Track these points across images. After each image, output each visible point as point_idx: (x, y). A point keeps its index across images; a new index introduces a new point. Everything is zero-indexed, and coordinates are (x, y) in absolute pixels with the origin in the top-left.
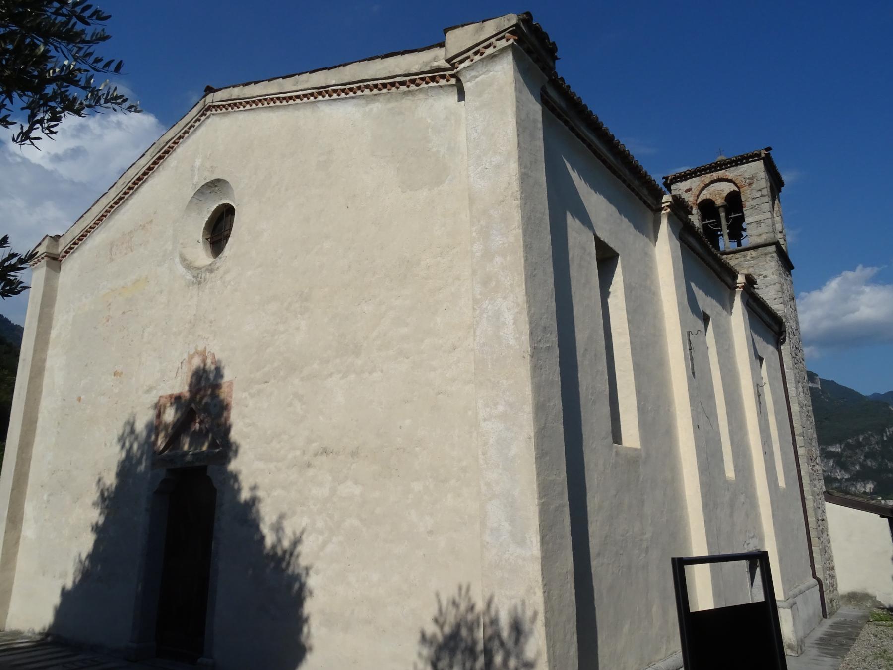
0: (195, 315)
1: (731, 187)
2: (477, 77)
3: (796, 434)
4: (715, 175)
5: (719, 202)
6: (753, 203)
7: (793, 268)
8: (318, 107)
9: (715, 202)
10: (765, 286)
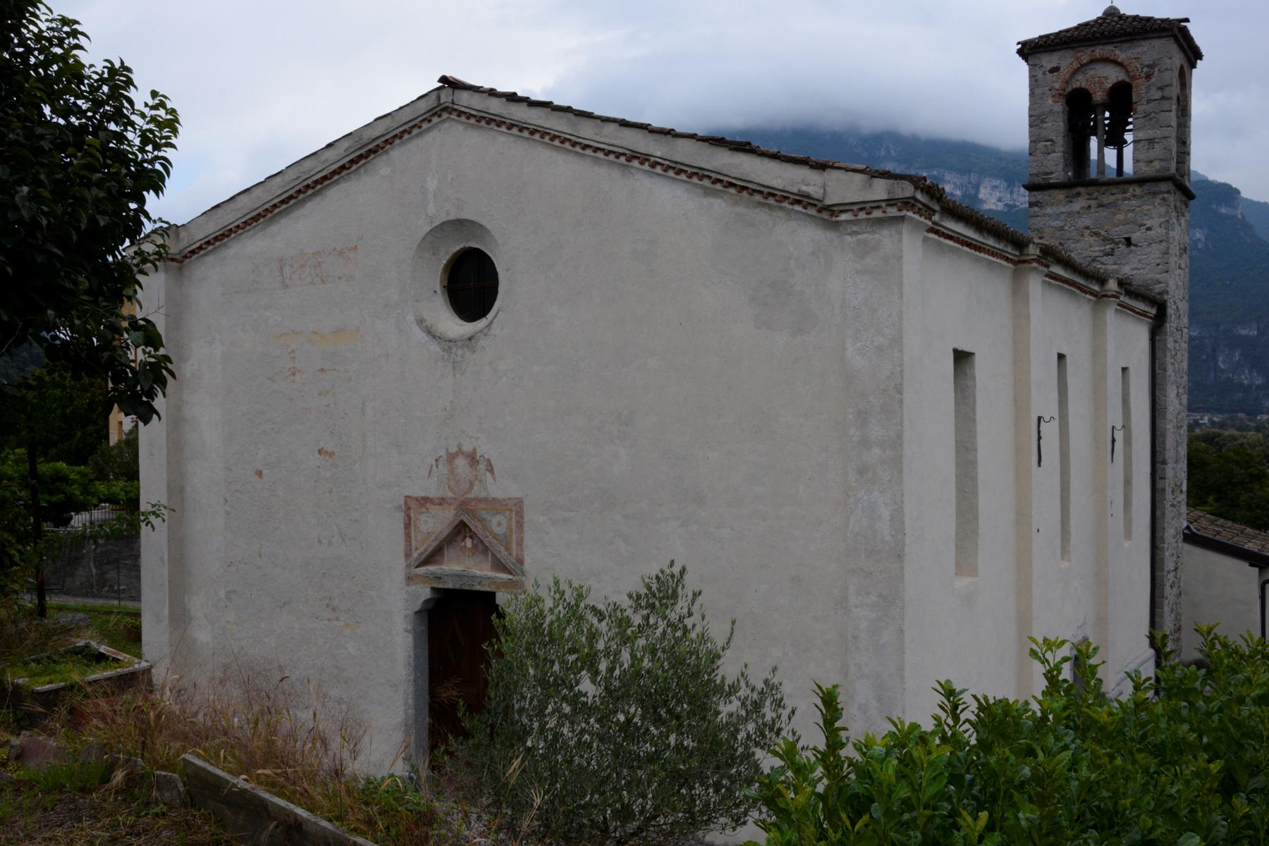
0: (451, 402)
2: (860, 234)
4: (1099, 51)
5: (1099, 96)
6: (1148, 108)
8: (631, 173)
9: (1093, 96)
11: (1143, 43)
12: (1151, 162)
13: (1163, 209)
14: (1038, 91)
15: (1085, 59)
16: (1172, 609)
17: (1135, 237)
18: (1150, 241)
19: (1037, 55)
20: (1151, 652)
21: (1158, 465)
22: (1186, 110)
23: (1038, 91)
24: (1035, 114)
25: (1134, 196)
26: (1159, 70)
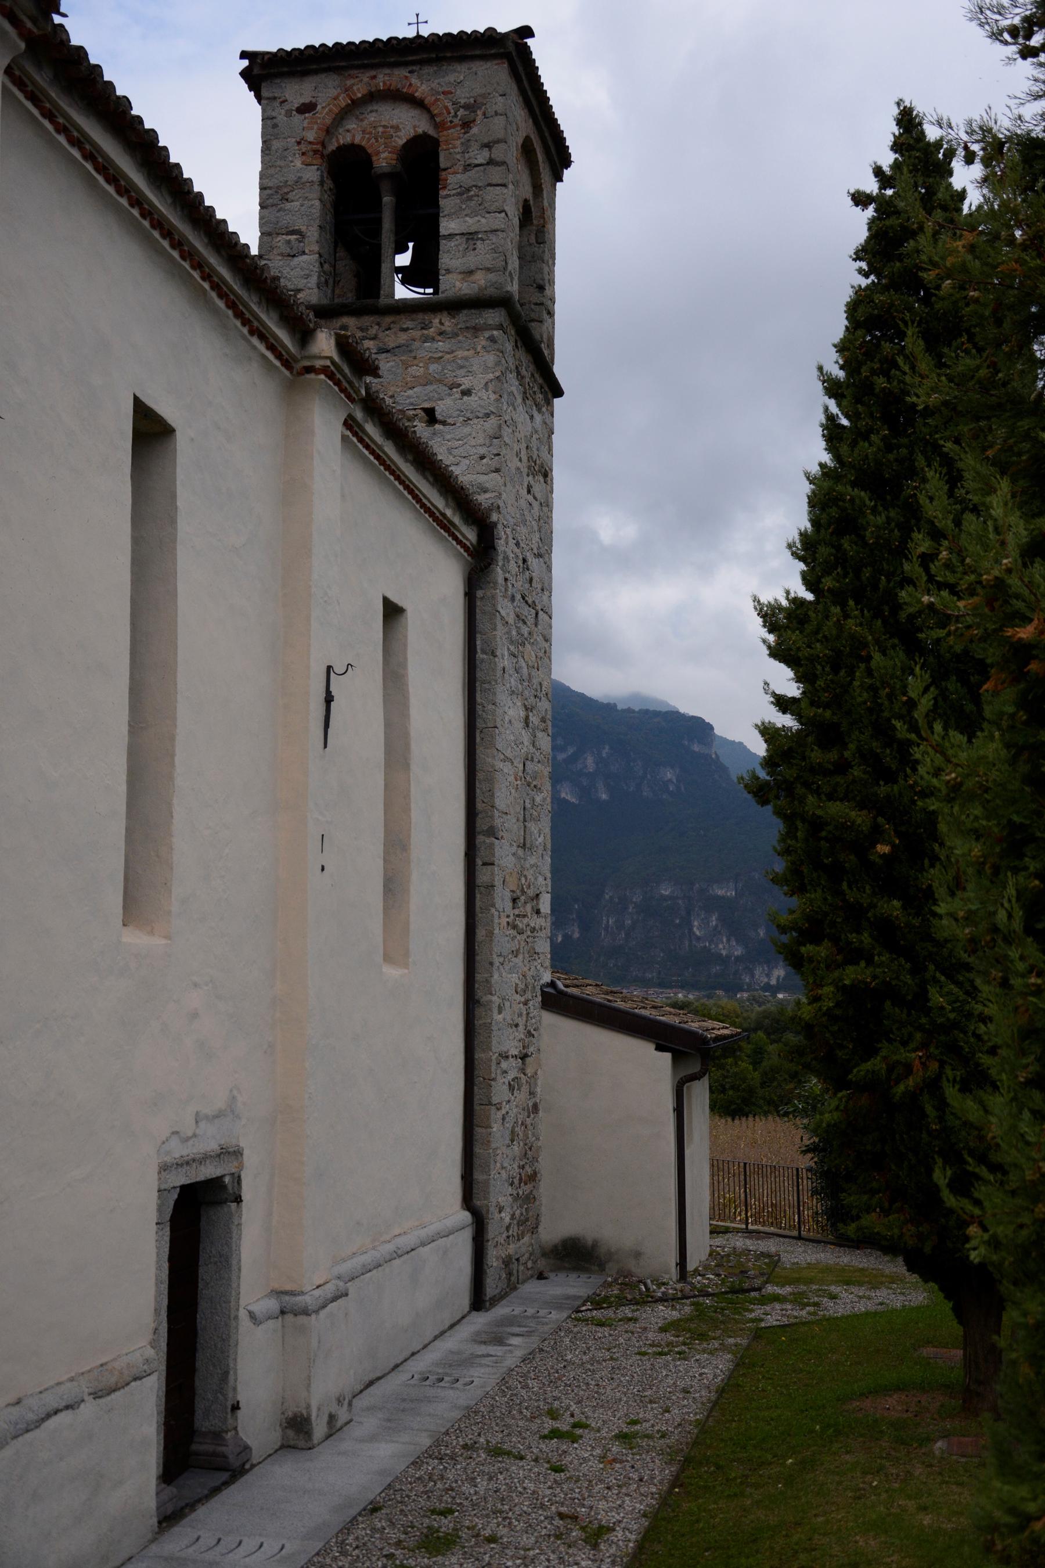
1: (423, 126)
3: (478, 829)
4: (384, 78)
5: (384, 160)
7: (558, 392)
9: (374, 158)
10: (461, 419)
11: (458, 67)
12: (471, 272)
13: (491, 359)
14: (276, 144)
15: (360, 90)
16: (513, 1133)
17: (441, 409)
18: (468, 415)
19: (278, 81)
20: (466, 1216)
21: (480, 839)
22: (543, 232)
23: (276, 144)
24: (270, 184)
25: (441, 334)
26: (484, 114)
